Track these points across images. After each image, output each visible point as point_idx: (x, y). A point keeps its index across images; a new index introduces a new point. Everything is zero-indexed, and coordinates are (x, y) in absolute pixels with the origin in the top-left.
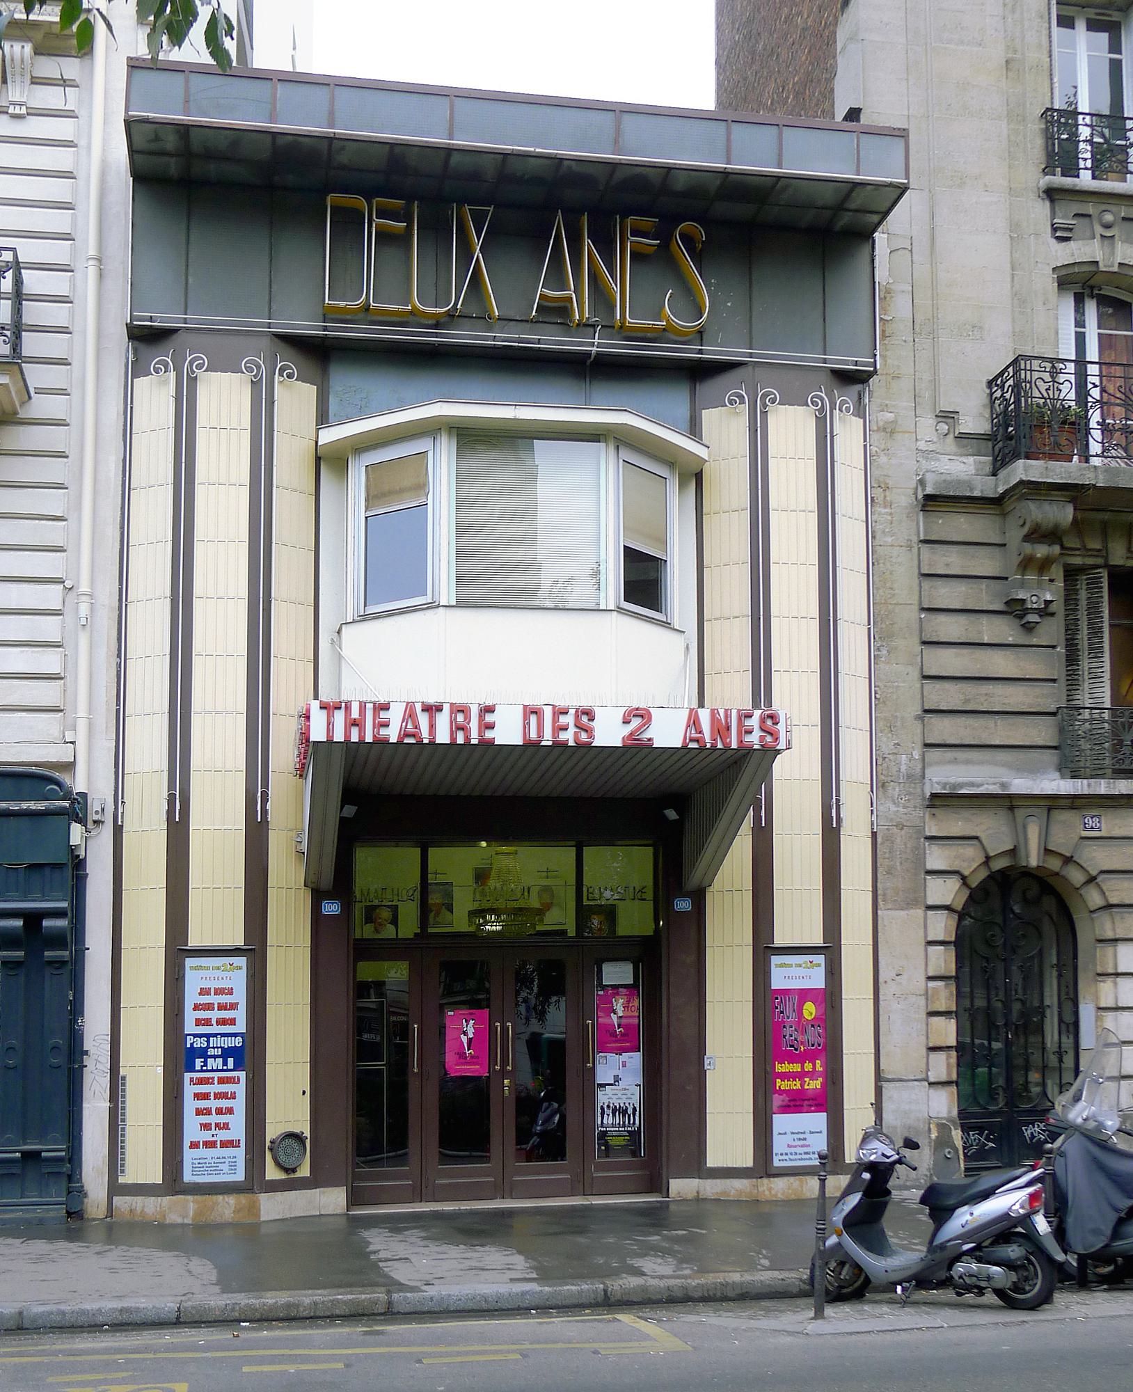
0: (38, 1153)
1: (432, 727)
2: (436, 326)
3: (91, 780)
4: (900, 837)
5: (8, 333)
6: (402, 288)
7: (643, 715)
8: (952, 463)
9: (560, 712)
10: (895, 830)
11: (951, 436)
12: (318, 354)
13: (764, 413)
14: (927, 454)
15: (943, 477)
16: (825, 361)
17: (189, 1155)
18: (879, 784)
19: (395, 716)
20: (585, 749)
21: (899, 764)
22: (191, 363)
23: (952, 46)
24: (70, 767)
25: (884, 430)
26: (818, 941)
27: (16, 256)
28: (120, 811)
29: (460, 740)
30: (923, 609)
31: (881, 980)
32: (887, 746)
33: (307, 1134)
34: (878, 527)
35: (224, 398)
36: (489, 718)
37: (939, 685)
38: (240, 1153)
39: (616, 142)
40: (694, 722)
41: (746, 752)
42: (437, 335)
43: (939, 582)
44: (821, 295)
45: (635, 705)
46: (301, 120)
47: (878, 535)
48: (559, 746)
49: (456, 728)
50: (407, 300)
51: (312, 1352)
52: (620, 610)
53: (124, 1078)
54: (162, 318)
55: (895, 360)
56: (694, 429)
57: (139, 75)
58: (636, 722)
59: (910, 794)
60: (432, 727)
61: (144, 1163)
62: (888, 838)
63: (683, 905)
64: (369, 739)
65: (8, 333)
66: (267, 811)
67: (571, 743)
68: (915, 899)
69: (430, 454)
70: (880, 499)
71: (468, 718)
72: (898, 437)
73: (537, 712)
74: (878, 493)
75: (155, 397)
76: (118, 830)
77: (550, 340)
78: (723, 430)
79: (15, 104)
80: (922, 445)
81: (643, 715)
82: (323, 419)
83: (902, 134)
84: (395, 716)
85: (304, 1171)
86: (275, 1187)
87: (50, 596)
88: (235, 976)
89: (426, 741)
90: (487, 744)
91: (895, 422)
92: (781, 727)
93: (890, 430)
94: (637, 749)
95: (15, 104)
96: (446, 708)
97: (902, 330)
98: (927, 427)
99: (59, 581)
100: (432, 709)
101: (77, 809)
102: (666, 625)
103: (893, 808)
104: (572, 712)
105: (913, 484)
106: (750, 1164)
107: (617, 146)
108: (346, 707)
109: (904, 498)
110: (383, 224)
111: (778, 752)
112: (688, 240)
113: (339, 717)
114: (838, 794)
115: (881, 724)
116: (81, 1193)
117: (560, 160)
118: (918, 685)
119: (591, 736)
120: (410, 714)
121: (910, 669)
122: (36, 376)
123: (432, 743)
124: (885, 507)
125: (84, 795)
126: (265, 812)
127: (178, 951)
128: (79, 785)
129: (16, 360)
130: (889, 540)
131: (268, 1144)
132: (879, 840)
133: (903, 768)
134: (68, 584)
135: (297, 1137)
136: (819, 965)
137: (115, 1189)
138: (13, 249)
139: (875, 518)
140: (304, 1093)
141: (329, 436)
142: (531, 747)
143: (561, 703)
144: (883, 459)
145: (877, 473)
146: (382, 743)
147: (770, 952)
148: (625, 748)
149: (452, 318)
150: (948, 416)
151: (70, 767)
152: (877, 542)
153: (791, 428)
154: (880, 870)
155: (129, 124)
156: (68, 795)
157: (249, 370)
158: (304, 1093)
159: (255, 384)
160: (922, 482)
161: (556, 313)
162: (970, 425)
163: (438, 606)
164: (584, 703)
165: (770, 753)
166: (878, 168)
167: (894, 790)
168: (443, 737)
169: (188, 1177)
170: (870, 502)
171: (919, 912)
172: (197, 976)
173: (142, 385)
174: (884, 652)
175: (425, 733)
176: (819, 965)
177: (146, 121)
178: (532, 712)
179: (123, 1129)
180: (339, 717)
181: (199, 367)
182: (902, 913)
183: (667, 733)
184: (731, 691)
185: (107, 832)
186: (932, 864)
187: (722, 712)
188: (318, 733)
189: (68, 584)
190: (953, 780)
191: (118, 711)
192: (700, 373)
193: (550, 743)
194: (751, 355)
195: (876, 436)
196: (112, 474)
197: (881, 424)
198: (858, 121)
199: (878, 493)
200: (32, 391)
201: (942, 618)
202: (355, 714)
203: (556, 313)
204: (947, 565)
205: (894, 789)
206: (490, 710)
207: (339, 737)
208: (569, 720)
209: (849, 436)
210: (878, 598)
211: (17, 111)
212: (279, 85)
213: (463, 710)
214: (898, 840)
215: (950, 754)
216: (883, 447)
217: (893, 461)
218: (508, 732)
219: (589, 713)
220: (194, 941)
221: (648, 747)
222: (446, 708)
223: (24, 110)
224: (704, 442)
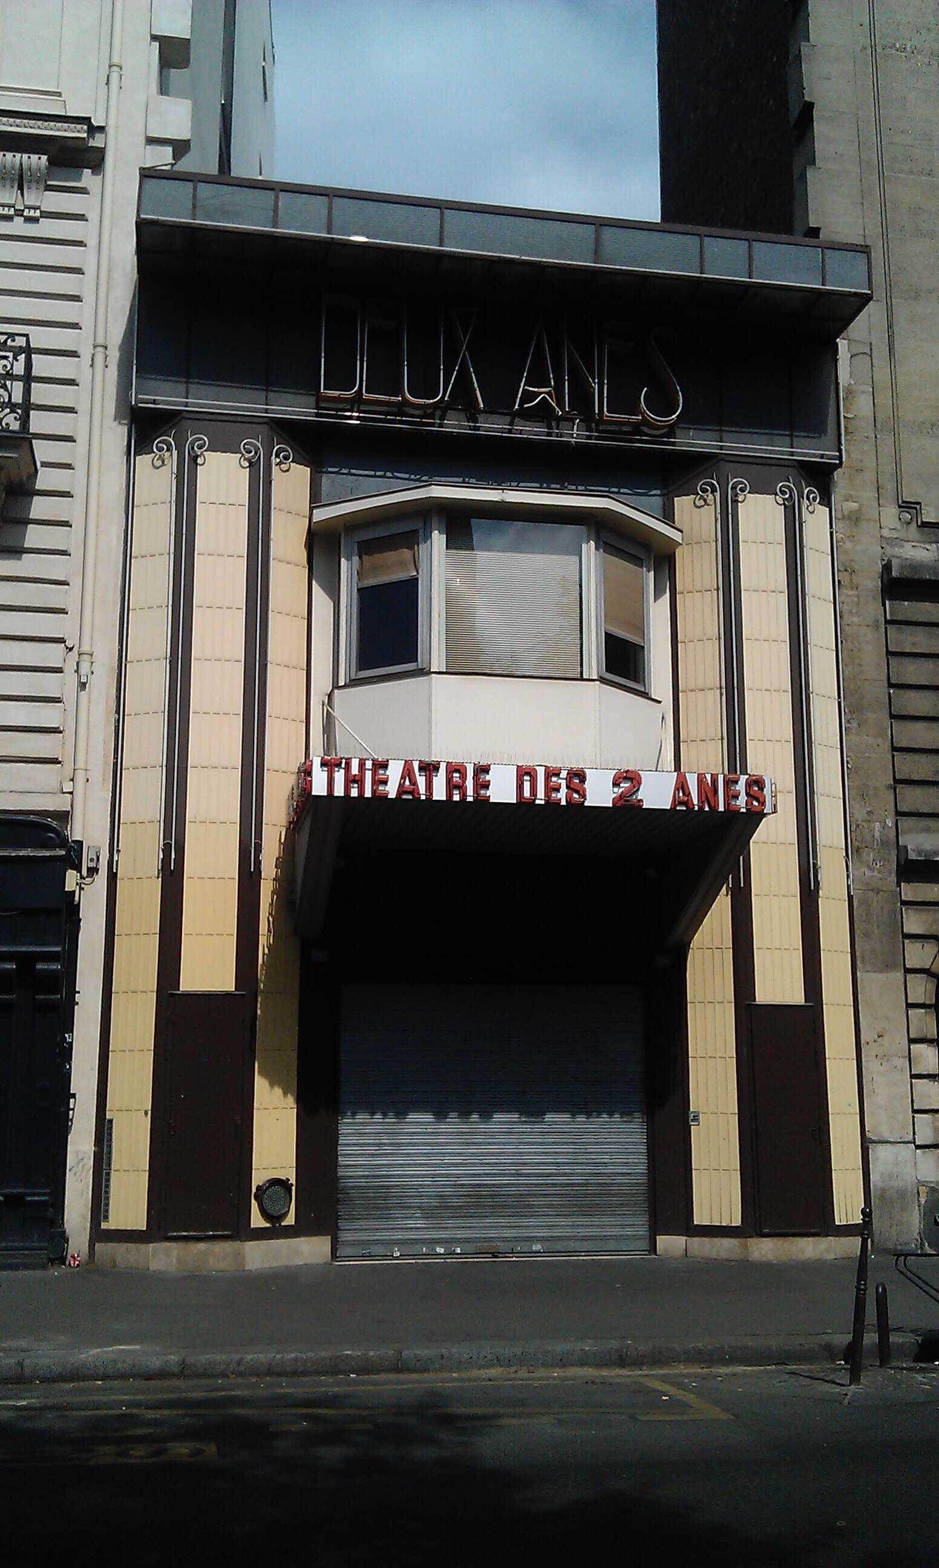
0: (22, 1196)
3: (89, 828)
4: (876, 900)
5: (19, 411)
7: (631, 778)
8: (916, 550)
9: (551, 773)
10: (871, 893)
11: (914, 525)
13: (735, 502)
14: (890, 541)
15: (908, 562)
16: (792, 454)
18: (853, 850)
19: (394, 773)
21: (872, 831)
23: (903, 176)
24: (64, 817)
25: (849, 518)
27: (28, 341)
28: (116, 858)
29: (456, 798)
30: (891, 685)
31: (862, 1041)
32: (860, 814)
33: (293, 1181)
34: (846, 608)
35: (223, 476)
37: (908, 757)
39: (596, 252)
40: (682, 785)
41: (731, 813)
43: (906, 661)
45: (624, 768)
46: (302, 223)
47: (845, 617)
48: (551, 805)
49: (451, 786)
50: (398, 391)
51: (304, 1411)
52: (602, 680)
53: (111, 1121)
55: (859, 456)
56: (668, 516)
57: (150, 183)
58: (625, 785)
59: (884, 859)
61: (129, 1207)
62: (865, 902)
65: (19, 411)
66: (260, 862)
68: (893, 961)
69: (421, 531)
70: (846, 582)
71: (463, 777)
72: (863, 525)
73: (531, 773)
74: (845, 577)
75: (156, 477)
76: (112, 878)
78: (693, 518)
79: (29, 208)
80: (886, 532)
81: (631, 778)
82: (315, 500)
83: (864, 250)
84: (394, 773)
85: (290, 1220)
86: (260, 1234)
87: (51, 655)
89: (423, 797)
90: (482, 802)
91: (859, 510)
92: (767, 791)
93: (854, 518)
94: (627, 809)
95: (29, 208)
96: (443, 766)
97: (864, 428)
98: (890, 514)
99: (62, 641)
100: (430, 769)
101: (73, 855)
102: (645, 695)
103: (868, 873)
104: (564, 774)
105: (879, 568)
106: (737, 1222)
107: (597, 256)
109: (872, 583)
111: (765, 815)
114: (815, 857)
115: (853, 793)
116: (64, 1238)
118: (890, 757)
119: (584, 797)
120: (408, 772)
121: (880, 741)
122: (43, 451)
124: (852, 589)
125: (80, 843)
126: (258, 863)
128: (76, 832)
129: (23, 439)
130: (856, 620)
131: (254, 1190)
132: (855, 903)
133: (877, 835)
134: (69, 644)
135: (283, 1184)
137: (98, 1235)
138: (27, 336)
139: (843, 598)
141: (320, 515)
142: (524, 806)
143: (552, 765)
144: (848, 545)
145: (842, 557)
146: (379, 799)
149: (427, 412)
150: (907, 506)
151: (64, 817)
152: (845, 621)
153: (760, 515)
154: (857, 932)
155: (141, 226)
156: (63, 842)
160: (887, 567)
162: (933, 514)
163: (430, 673)
164: (575, 765)
165: (754, 817)
166: (845, 278)
167: (870, 856)
168: (440, 793)
170: (837, 585)
171: (899, 975)
173: (143, 462)
174: (854, 724)
175: (422, 789)
177: (155, 223)
178: (525, 773)
179: (108, 1174)
180: (339, 776)
181: (742, 490)
182: (880, 976)
183: (656, 794)
184: (707, 758)
185: (102, 878)
186: (911, 927)
187: (709, 777)
188: (319, 788)
190: (927, 847)
191: (115, 764)
193: (543, 802)
194: (721, 448)
195: (841, 524)
197: (846, 513)
198: (818, 237)
199: (845, 577)
200: (38, 464)
201: (911, 694)
202: (355, 770)
204: (914, 644)
205: (868, 854)
206: (485, 770)
207: (339, 791)
209: (816, 522)
210: (847, 673)
211: (32, 213)
213: (460, 769)
214: (875, 904)
215: (924, 823)
216: (848, 534)
217: (859, 547)
218: (502, 790)
219: (581, 776)
221: (638, 806)
222: (443, 766)
223: (38, 213)
224: (677, 525)
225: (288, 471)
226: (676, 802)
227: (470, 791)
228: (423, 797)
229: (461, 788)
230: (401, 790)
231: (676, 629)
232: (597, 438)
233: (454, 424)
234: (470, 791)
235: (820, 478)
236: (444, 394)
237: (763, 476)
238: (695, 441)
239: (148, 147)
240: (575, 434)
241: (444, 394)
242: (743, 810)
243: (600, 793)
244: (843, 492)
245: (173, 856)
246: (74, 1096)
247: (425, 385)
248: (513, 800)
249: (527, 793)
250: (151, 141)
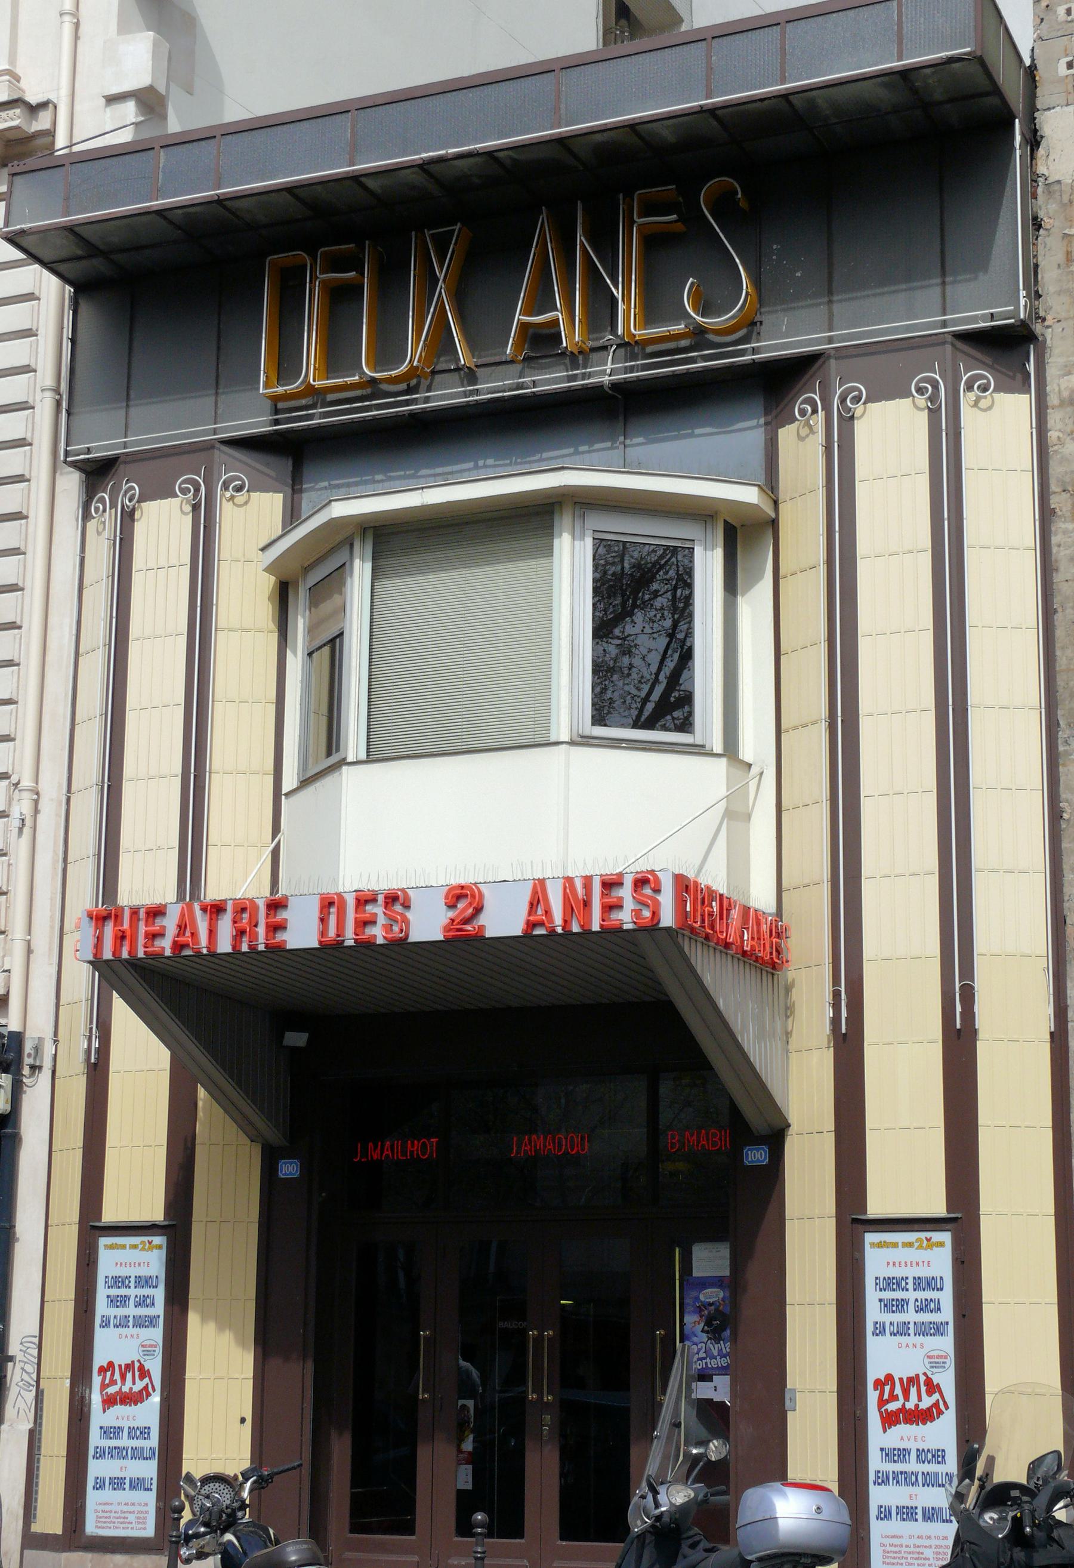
1: (212, 933)
2: (409, 391)
6: (429, 348)
9: (610, 884)
12: (294, 453)
17: (93, 1498)
19: (170, 923)
20: (400, 945)
22: (843, 400)
26: (938, 1207)
29: (245, 948)
36: (283, 915)
38: (150, 1498)
42: (407, 403)
44: (214, 358)
45: (454, 881)
48: (366, 946)
54: (102, 448)
60: (212, 933)
63: (756, 1156)
64: (667, 919)
67: (380, 941)
77: (550, 380)
88: (937, 1258)
90: (277, 950)
104: (381, 898)
108: (116, 916)
110: (329, 280)
112: (723, 207)
113: (109, 930)
117: (490, 155)
123: (213, 954)
127: (92, 1229)
134: (14, 779)
136: (941, 1244)
140: (243, 1420)
142: (330, 949)
147: (860, 1227)
148: (446, 941)
149: (412, 382)
157: (185, 491)
158: (243, 1420)
159: (934, 413)
161: (542, 343)
164: (643, 866)
168: (224, 945)
169: (91, 1528)
172: (880, 1257)
176: (941, 1244)
178: (329, 904)
180: (109, 930)
181: (857, 400)
189: (14, 779)
192: (777, 385)
196: (66, 641)
203: (542, 343)
208: (626, 893)
212: (162, 152)
218: (504, 920)
220: (110, 1215)
221: (479, 938)
225: (246, 503)
226: (531, 925)
227: (261, 938)
228: (559, 930)
229: (254, 936)
230: (178, 947)
231: (743, 639)
232: (646, 367)
233: (447, 395)
234: (261, 938)
235: (1007, 348)
236: (414, 352)
237: (888, 370)
238: (777, 343)
239: (108, 109)
240: (607, 371)
241: (414, 352)
242: (630, 926)
243: (428, 925)
244: (1062, 360)
245: (959, 1009)
246: (11, 1359)
247: (388, 348)
248: (315, 944)
249: (332, 933)
250: (112, 99)
